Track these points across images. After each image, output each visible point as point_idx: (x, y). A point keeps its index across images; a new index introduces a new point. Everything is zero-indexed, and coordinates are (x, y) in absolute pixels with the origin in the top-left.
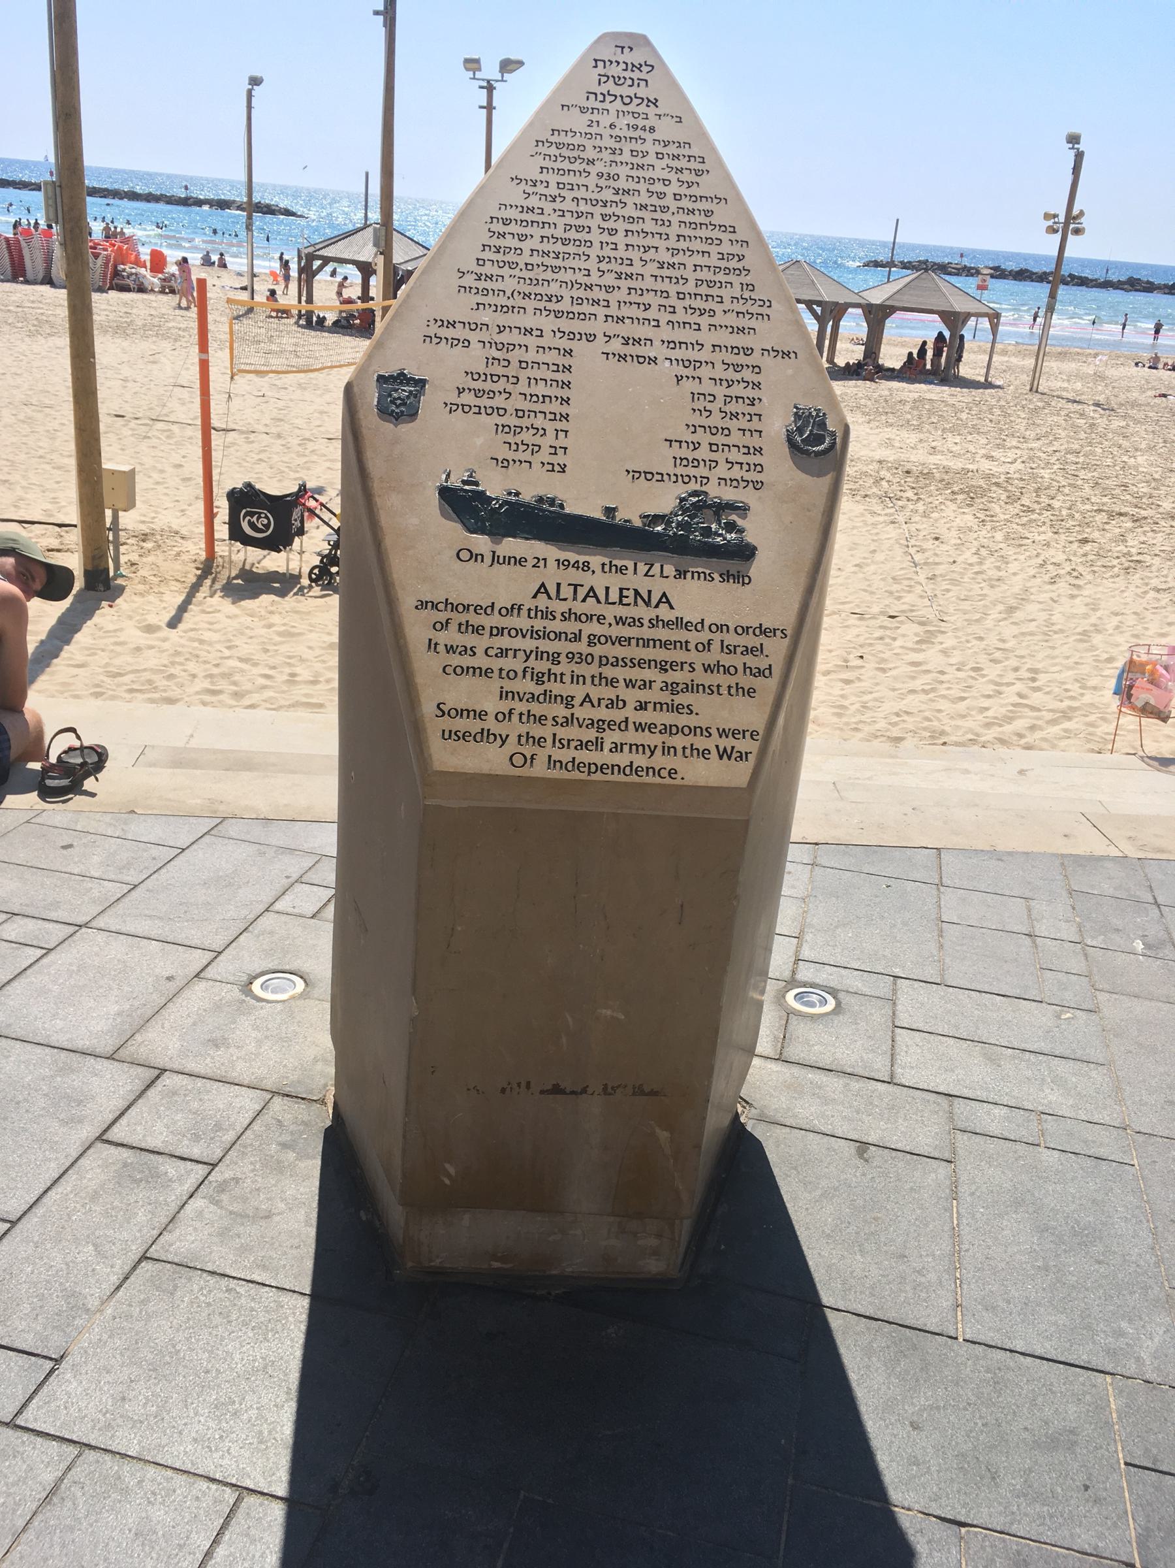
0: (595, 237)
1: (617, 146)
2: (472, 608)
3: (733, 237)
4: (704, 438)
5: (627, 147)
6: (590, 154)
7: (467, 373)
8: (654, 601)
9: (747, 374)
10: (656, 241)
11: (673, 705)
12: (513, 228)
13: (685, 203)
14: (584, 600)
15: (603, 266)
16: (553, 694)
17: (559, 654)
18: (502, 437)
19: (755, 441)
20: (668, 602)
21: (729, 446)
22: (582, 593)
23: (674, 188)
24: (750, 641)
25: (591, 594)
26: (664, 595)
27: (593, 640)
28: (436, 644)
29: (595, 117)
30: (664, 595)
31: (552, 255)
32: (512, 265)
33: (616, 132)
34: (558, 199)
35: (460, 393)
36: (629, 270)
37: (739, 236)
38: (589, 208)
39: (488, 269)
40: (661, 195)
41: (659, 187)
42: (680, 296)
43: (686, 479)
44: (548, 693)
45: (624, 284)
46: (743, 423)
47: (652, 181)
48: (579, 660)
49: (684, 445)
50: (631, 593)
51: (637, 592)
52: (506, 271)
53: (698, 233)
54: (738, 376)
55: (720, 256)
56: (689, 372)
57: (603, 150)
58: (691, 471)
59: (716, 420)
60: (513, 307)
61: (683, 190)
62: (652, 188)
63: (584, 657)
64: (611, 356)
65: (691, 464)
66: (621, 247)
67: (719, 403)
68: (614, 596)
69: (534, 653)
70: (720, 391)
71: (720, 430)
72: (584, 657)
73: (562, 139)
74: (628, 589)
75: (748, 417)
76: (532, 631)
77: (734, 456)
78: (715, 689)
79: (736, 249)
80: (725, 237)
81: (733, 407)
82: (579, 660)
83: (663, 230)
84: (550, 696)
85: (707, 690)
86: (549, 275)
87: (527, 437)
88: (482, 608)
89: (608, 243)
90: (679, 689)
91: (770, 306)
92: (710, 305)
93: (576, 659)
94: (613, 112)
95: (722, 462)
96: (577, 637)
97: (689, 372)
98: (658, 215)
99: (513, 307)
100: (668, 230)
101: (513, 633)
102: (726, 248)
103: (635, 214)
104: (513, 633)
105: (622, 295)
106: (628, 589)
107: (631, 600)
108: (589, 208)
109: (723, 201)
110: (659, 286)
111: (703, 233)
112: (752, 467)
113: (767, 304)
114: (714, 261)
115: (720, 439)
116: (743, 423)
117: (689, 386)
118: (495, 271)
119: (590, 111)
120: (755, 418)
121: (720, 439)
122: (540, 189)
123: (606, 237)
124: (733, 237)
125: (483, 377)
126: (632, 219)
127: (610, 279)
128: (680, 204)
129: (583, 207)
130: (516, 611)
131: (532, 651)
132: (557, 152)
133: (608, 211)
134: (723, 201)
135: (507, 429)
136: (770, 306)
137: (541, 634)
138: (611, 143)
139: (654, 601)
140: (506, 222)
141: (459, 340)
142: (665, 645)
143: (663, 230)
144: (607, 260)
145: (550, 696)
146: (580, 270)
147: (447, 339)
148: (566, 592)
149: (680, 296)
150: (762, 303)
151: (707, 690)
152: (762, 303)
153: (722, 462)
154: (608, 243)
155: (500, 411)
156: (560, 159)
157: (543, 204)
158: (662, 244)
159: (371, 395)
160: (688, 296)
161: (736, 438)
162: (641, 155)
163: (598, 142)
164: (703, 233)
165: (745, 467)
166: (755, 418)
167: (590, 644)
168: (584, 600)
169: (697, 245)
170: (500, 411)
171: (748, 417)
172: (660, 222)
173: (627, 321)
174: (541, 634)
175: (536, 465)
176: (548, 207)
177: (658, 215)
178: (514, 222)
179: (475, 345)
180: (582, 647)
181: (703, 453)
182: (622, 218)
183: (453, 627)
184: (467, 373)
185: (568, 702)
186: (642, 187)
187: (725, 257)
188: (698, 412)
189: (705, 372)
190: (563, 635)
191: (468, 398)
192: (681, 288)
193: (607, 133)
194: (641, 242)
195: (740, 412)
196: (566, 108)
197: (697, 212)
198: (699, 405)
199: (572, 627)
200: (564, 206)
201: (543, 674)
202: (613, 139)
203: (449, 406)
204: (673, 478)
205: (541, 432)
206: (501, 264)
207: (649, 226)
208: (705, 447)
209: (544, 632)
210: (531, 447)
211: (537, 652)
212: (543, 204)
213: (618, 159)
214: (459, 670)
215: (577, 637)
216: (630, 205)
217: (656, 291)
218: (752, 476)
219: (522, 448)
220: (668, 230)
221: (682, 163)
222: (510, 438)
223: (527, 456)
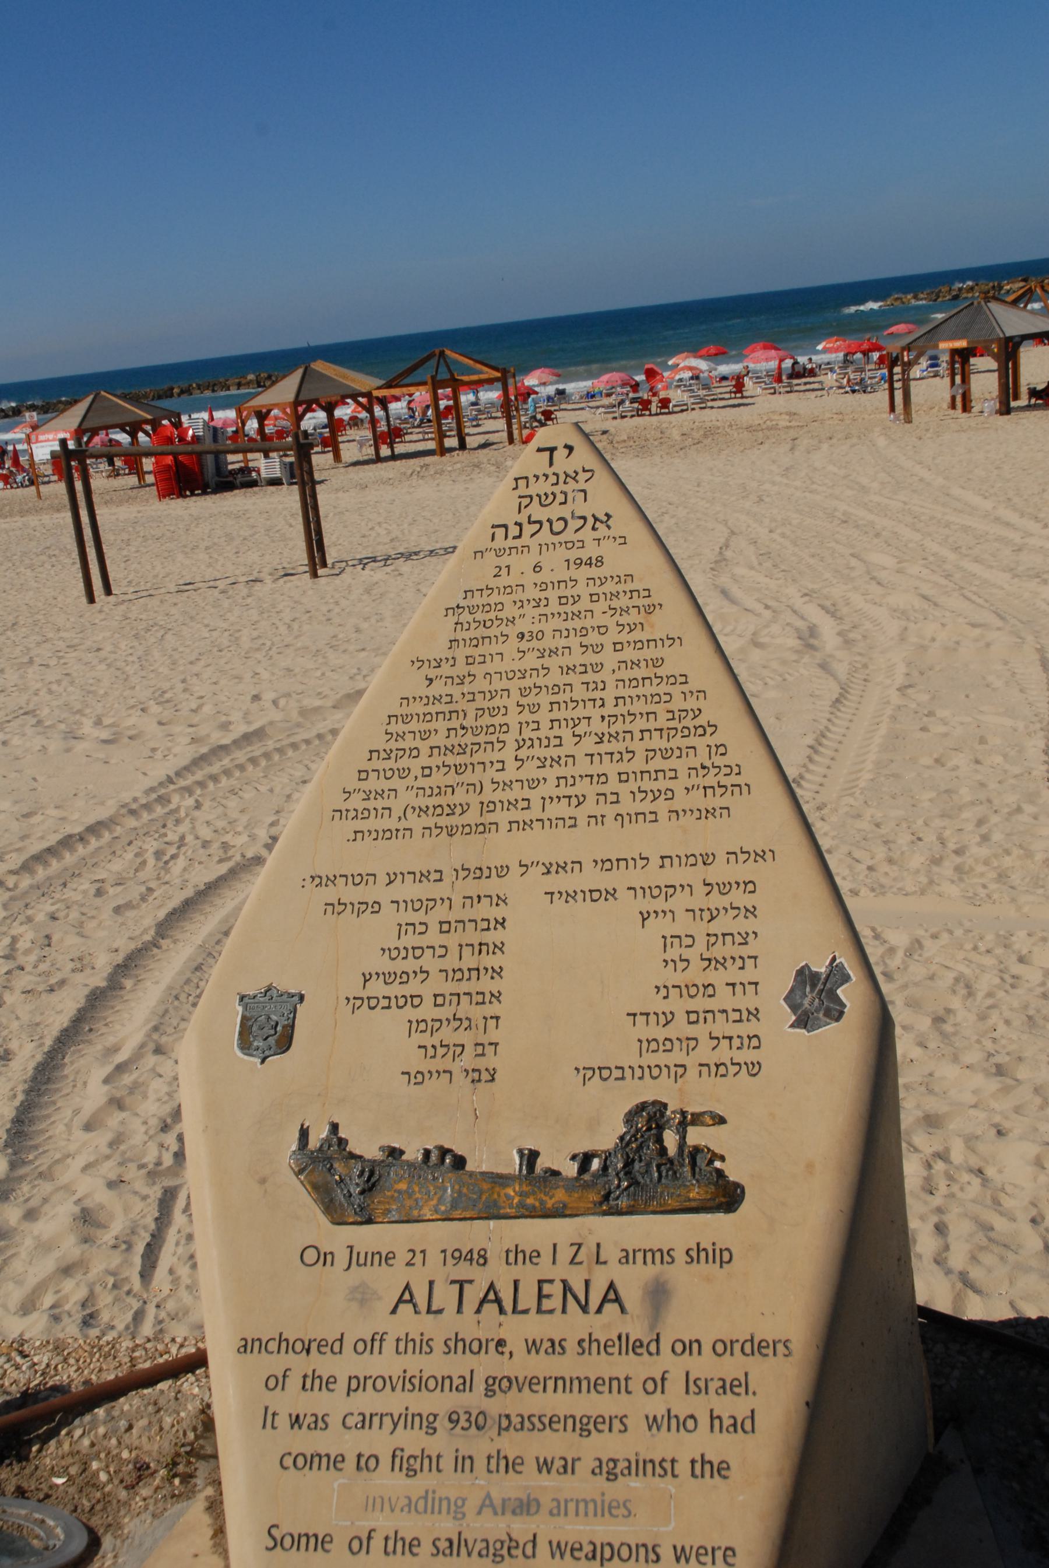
0: (513, 719)
1: (543, 595)
2: (737, 1347)
3: (685, 688)
4: (678, 1005)
5: (553, 595)
6: (510, 611)
7: (383, 950)
8: (594, 1304)
9: (738, 897)
10: (590, 710)
11: (603, 1501)
12: (414, 726)
13: (629, 654)
14: (599, 1311)
15: (523, 753)
16: (437, 1496)
17: (435, 1416)
18: (418, 1038)
19: (746, 1001)
20: (617, 1300)
21: (712, 1012)
22: (473, 1294)
23: (613, 635)
24: (732, 1367)
25: (491, 1296)
26: (612, 1286)
27: (493, 1386)
28: (274, 1414)
29: (505, 561)
30: (612, 1286)
31: (457, 749)
32: (403, 773)
33: (544, 576)
34: (468, 679)
35: (366, 981)
36: (554, 752)
37: (694, 685)
38: (505, 684)
39: (374, 783)
40: (598, 649)
41: (593, 638)
42: (623, 777)
43: (655, 1072)
44: (430, 1496)
45: (551, 773)
46: (732, 974)
47: (584, 632)
48: (467, 1425)
49: (653, 1018)
50: (557, 1289)
51: (567, 1288)
52: (396, 783)
53: (640, 691)
54: (724, 901)
55: (670, 716)
56: (659, 904)
57: (526, 603)
58: (661, 1058)
59: (695, 974)
60: (398, 830)
61: (624, 637)
62: (586, 641)
63: (473, 1419)
64: (556, 896)
65: (662, 1048)
66: (545, 725)
67: (700, 946)
68: (528, 1298)
69: (403, 1417)
70: (700, 929)
71: (702, 989)
72: (473, 1419)
73: (478, 600)
74: (551, 1281)
75: (739, 963)
76: (404, 1378)
77: (721, 1027)
78: (667, 1465)
79: (691, 704)
80: (676, 690)
81: (718, 951)
82: (467, 1425)
83: (597, 695)
84: (433, 1499)
85: (658, 1470)
86: (452, 778)
87: (446, 1034)
88: (641, 1346)
89: (528, 723)
90: (618, 1471)
91: (739, 774)
92: (662, 784)
93: (463, 1423)
94: (535, 549)
95: (704, 1039)
96: (466, 1384)
97: (659, 904)
98: (590, 677)
99: (398, 830)
100: (602, 694)
101: (379, 1384)
102: (677, 704)
103: (561, 680)
104: (379, 1384)
105: (548, 789)
106: (551, 1281)
107: (556, 1303)
108: (505, 684)
109: (678, 641)
110: (596, 769)
111: (648, 689)
112: (746, 1041)
113: (736, 770)
114: (662, 722)
115: (700, 1003)
116: (732, 974)
117: (658, 926)
118: (384, 785)
119: (508, 552)
120: (749, 963)
121: (700, 1003)
122: (446, 670)
123: (527, 716)
124: (685, 688)
125: (403, 953)
126: (556, 689)
127: (530, 771)
128: (621, 656)
129: (498, 684)
130: (377, 1344)
131: (400, 1415)
132: (470, 618)
133: (528, 682)
134: (678, 641)
135: (422, 1026)
136: (739, 774)
137: (416, 1381)
138: (536, 594)
139: (594, 1304)
140: (406, 719)
141: (367, 903)
142: (595, 1385)
143: (597, 695)
144: (529, 743)
145: (433, 1499)
146: (492, 763)
147: (352, 904)
148: (446, 1297)
149: (623, 777)
150: (728, 770)
151: (658, 1470)
152: (728, 770)
153: (704, 1039)
154: (528, 723)
155: (413, 1000)
156: (473, 625)
157: (449, 690)
158: (595, 713)
159: (651, 1109)
160: (632, 776)
161: (724, 999)
162: (571, 601)
163: (519, 595)
164: (648, 689)
165: (736, 1042)
166: (749, 963)
167: (489, 1392)
168: (599, 1311)
169: (638, 707)
170: (413, 1000)
171: (739, 963)
172: (592, 686)
173: (535, 825)
174: (416, 1381)
175: (458, 1076)
176: (456, 690)
177: (590, 677)
178: (415, 718)
179: (388, 909)
180: (475, 1400)
181: (680, 1028)
182: (544, 689)
183: (294, 1382)
184: (383, 950)
185: (457, 1510)
186: (574, 641)
187: (677, 716)
188: (671, 965)
189: (680, 901)
190: (447, 1382)
191: (377, 988)
192: (623, 767)
193: (530, 578)
194: (569, 714)
195: (728, 957)
196: (479, 555)
197: (643, 664)
198: (673, 953)
199: (458, 1365)
200: (476, 687)
201: (415, 1458)
202: (538, 588)
203: (582, 1072)
204: (638, 1072)
205: (466, 1024)
206: (389, 774)
207: (579, 692)
208: (681, 1018)
209: (421, 1378)
210: (452, 1049)
211: (406, 1415)
212: (449, 690)
213: (547, 611)
214: (300, 1461)
215: (466, 1384)
216: (555, 671)
217: (592, 776)
218: (747, 1055)
219: (441, 1051)
220: (602, 694)
221: (624, 601)
222: (427, 1040)
223: (447, 1064)
